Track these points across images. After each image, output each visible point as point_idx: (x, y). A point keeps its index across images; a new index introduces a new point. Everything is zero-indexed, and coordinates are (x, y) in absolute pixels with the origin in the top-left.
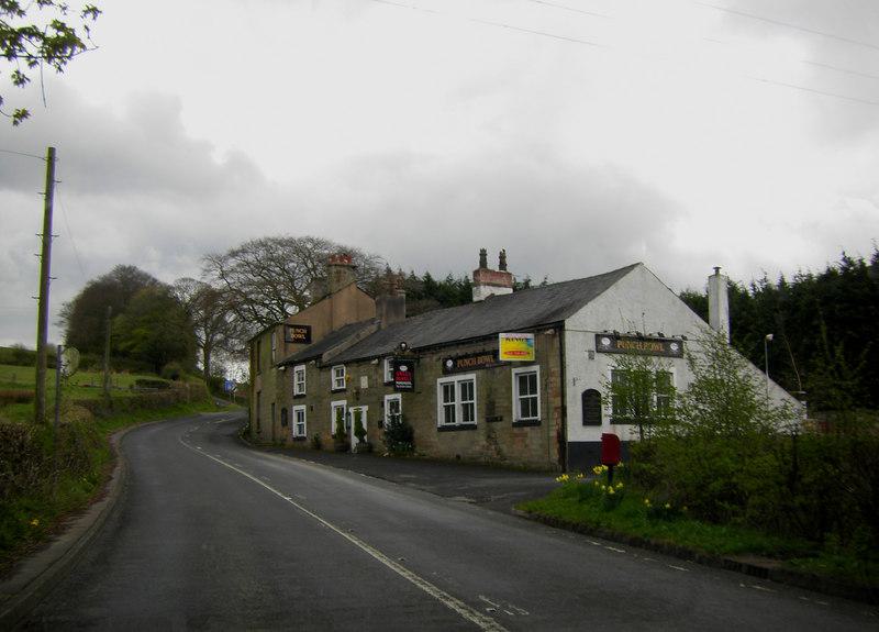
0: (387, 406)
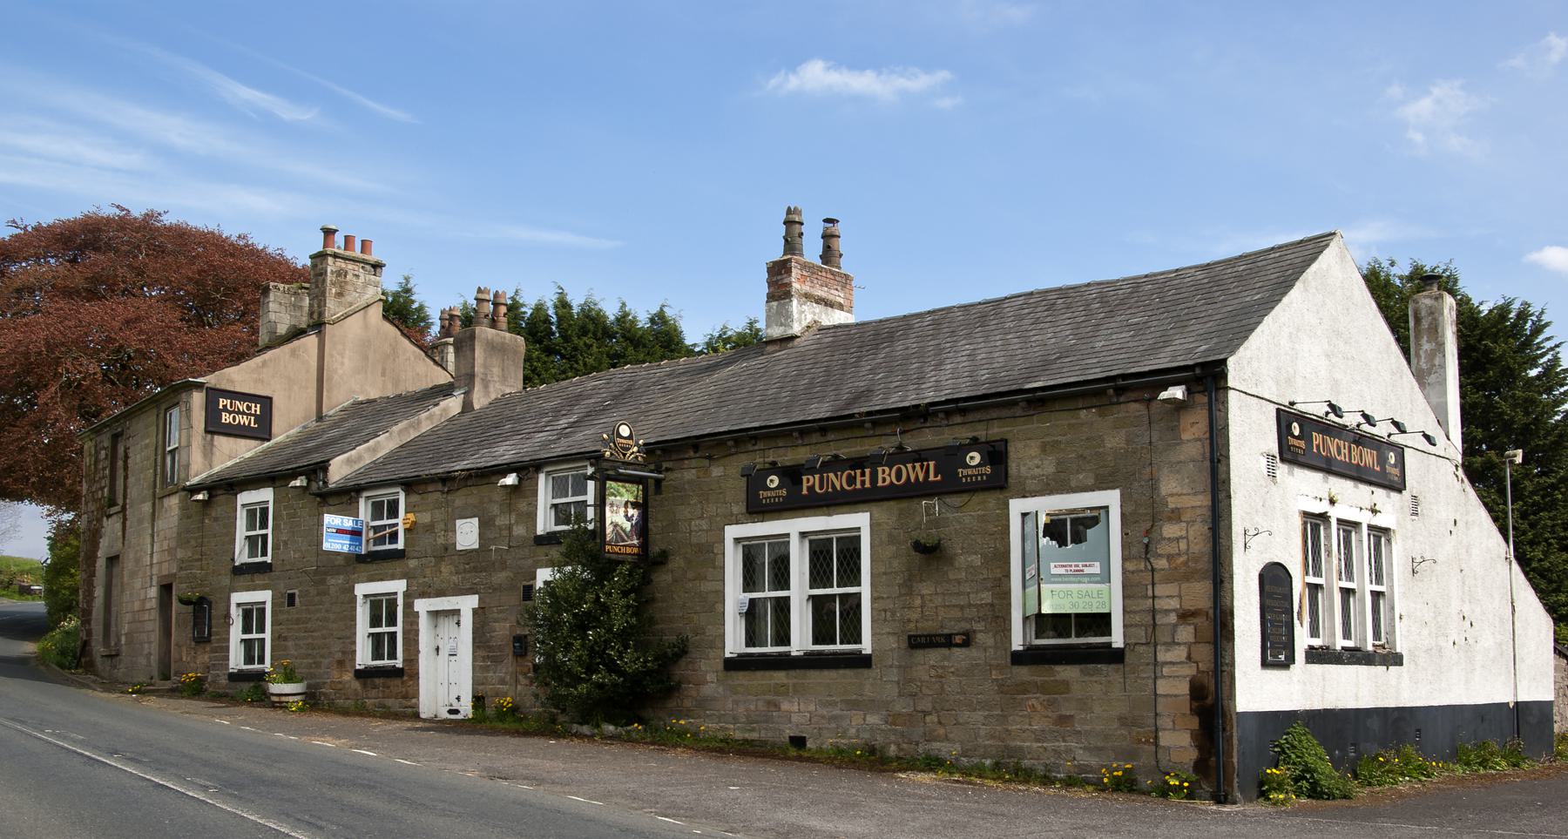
0: (362, 614)
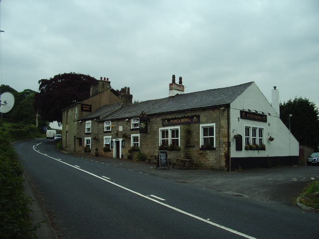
0: (132, 139)
